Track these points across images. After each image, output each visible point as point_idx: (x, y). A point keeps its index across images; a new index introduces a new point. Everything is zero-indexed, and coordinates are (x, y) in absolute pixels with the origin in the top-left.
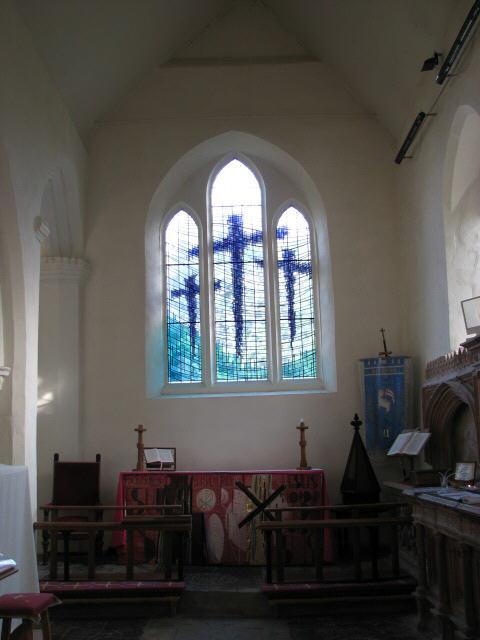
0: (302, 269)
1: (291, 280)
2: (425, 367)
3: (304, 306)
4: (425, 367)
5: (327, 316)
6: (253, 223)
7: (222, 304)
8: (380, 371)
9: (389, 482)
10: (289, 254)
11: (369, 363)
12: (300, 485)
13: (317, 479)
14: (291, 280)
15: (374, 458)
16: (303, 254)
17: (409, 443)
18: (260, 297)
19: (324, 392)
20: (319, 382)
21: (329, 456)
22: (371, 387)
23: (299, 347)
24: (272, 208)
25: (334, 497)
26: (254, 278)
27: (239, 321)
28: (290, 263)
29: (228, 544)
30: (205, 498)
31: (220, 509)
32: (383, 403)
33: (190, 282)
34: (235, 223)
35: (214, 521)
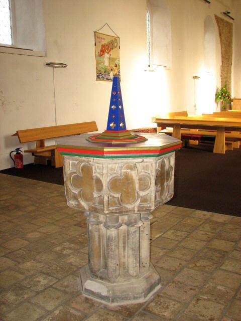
19: (137, 186)
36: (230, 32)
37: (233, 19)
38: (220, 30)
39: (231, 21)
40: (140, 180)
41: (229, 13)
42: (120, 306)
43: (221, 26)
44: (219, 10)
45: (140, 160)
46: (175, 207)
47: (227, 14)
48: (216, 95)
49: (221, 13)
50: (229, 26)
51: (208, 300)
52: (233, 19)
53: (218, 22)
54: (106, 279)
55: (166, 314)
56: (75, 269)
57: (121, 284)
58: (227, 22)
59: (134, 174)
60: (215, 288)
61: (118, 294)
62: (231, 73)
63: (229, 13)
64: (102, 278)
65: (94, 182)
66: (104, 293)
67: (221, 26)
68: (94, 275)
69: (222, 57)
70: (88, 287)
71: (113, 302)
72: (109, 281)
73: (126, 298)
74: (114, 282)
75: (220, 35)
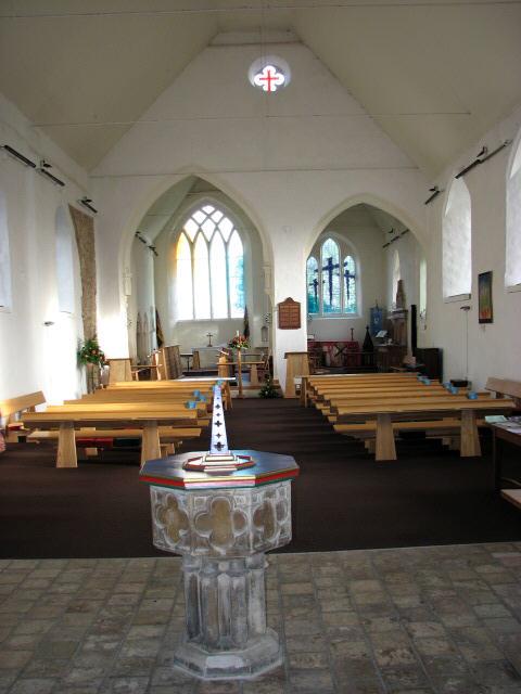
0: (352, 277)
1: (348, 281)
2: (173, 323)
3: (352, 290)
4: (173, 323)
5: (360, 293)
6: (336, 261)
7: (326, 286)
8: (375, 312)
9: (376, 344)
10: (347, 272)
11: (372, 309)
12: (351, 345)
13: (356, 343)
14: (348, 281)
15: (372, 338)
16: (352, 271)
17: (382, 334)
18: (338, 286)
19: (275, 515)
20: (356, 315)
21: (360, 337)
22: (372, 317)
23: (350, 302)
24: (343, 256)
25: (361, 347)
26: (336, 280)
27: (331, 294)
28: (347, 274)
29: (332, 362)
30: (325, 349)
31: (329, 352)
32: (376, 322)
33: (315, 281)
34: (330, 260)
35: (328, 355)
36: (91, 235)
37: (95, 211)
38: (77, 233)
39: (91, 214)
40: (277, 507)
41: (89, 201)
42: (263, 675)
43: (78, 223)
44: (72, 196)
45: (278, 485)
46: (66, 561)
47: (86, 202)
48: (79, 354)
49: (77, 201)
50: (88, 222)
51: (344, 642)
52: (95, 211)
53: (73, 217)
54: (233, 647)
55: (317, 665)
56: (153, 660)
57: (256, 648)
58: (86, 217)
59: (274, 502)
60: (338, 630)
61: (256, 660)
62: (95, 310)
63: (89, 201)
64: (226, 649)
65: (232, 518)
66: (240, 664)
67: (78, 223)
68: (213, 647)
69: (83, 281)
70: (212, 666)
71: (252, 672)
72: (239, 648)
73: (264, 663)
74: (245, 648)
75: (78, 240)
